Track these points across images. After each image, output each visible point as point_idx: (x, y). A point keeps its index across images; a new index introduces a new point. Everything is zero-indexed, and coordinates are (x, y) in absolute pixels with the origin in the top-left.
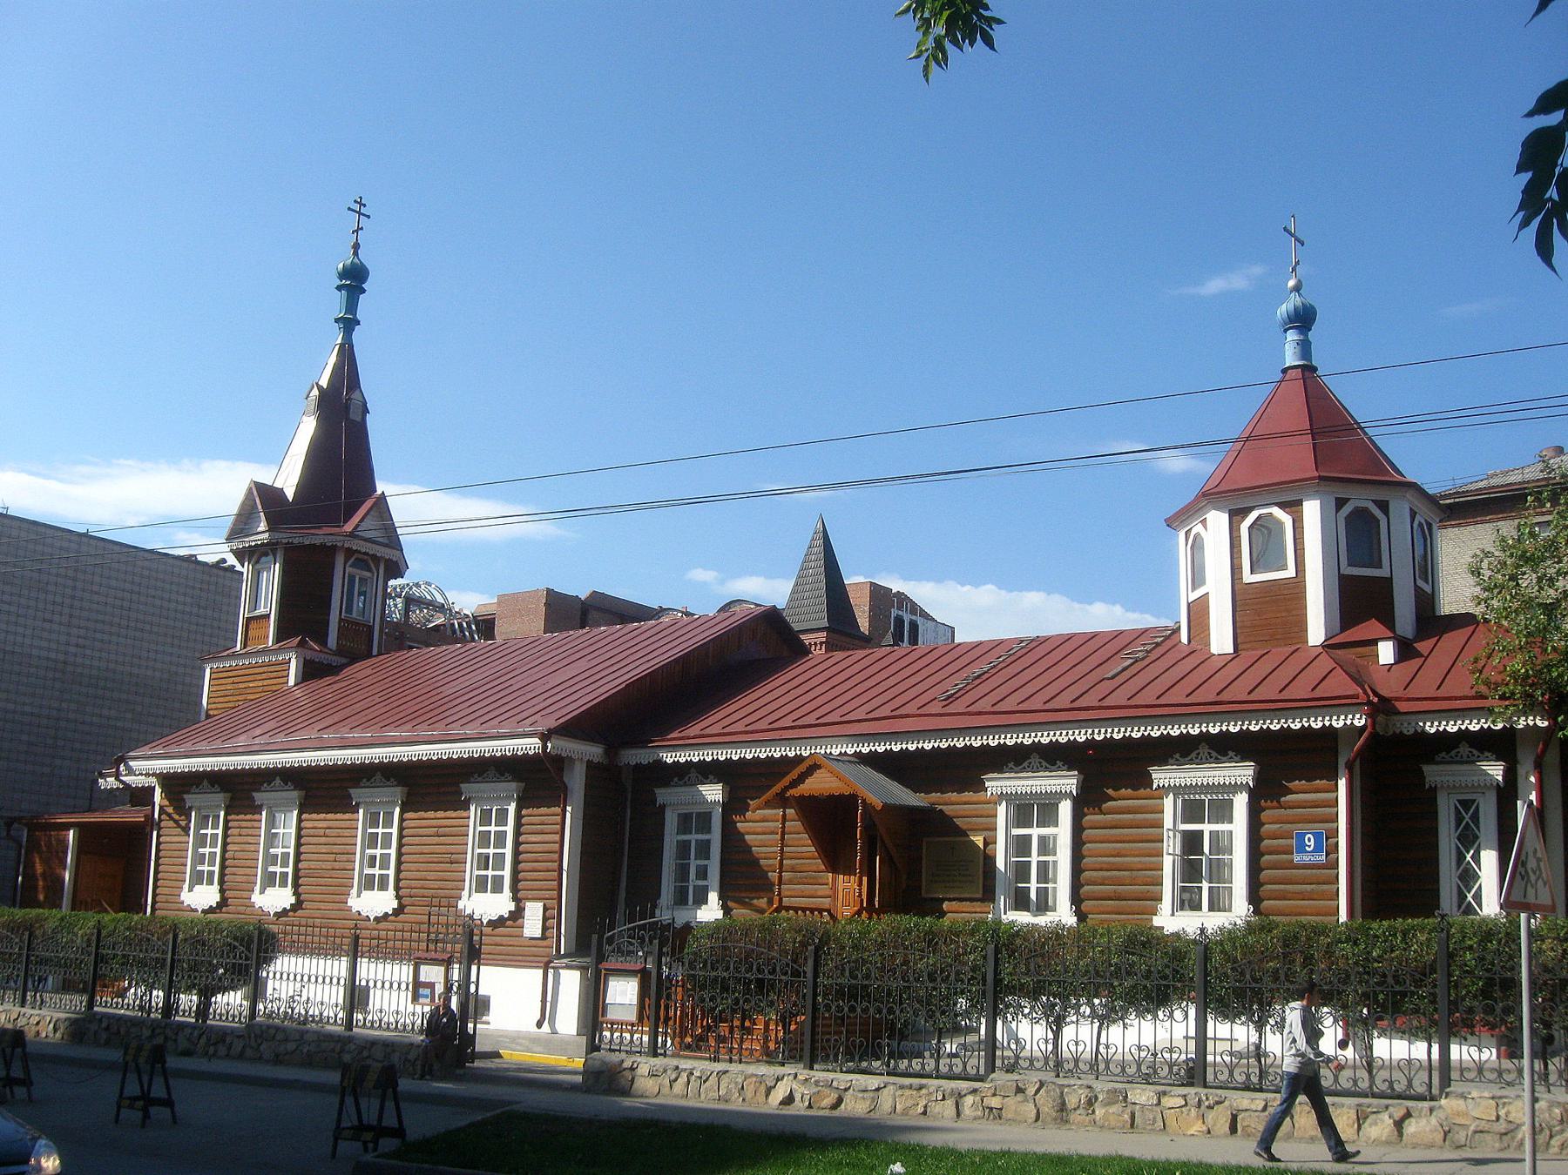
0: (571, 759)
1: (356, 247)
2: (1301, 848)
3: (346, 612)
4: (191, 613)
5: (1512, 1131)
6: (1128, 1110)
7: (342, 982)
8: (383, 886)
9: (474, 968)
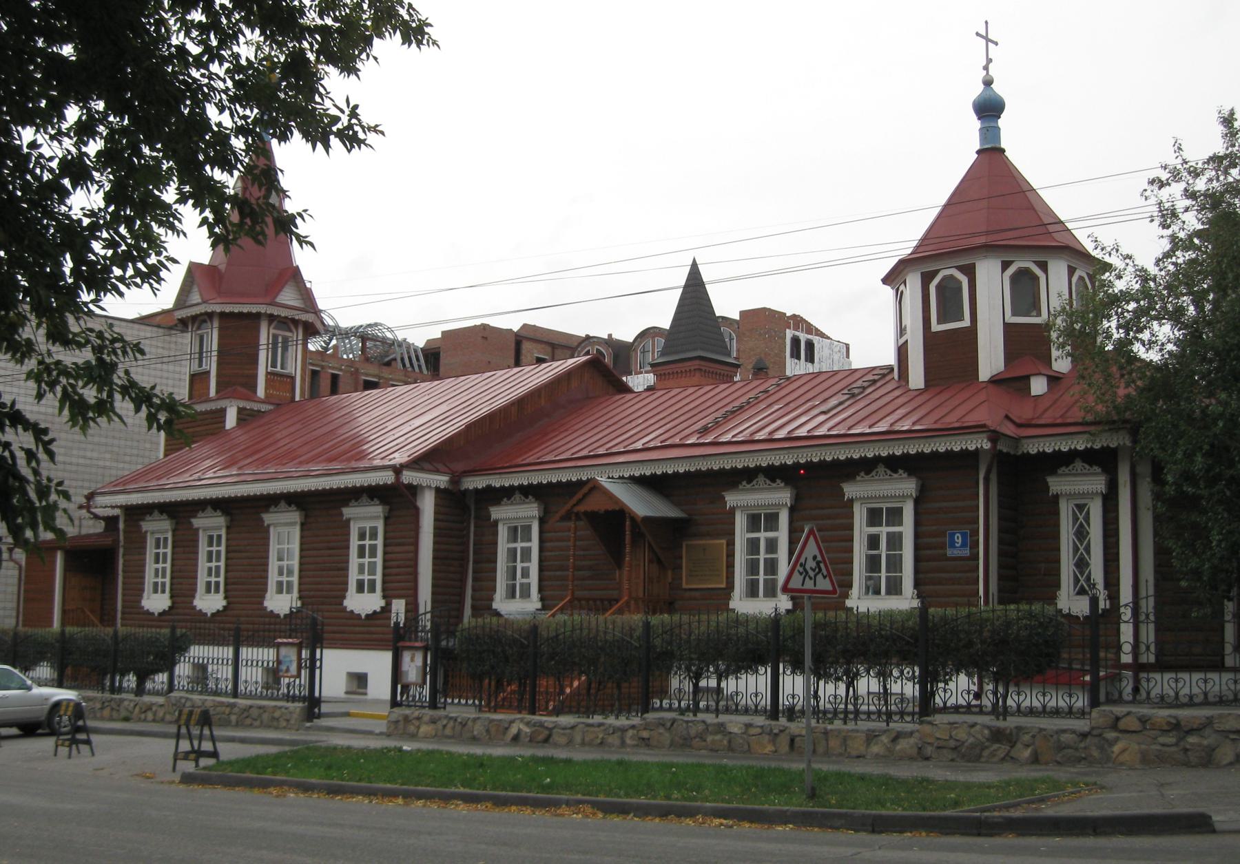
2: (952, 545)
5: (959, 746)
6: (727, 738)
7: (230, 662)
8: (372, 589)
9: (318, 651)
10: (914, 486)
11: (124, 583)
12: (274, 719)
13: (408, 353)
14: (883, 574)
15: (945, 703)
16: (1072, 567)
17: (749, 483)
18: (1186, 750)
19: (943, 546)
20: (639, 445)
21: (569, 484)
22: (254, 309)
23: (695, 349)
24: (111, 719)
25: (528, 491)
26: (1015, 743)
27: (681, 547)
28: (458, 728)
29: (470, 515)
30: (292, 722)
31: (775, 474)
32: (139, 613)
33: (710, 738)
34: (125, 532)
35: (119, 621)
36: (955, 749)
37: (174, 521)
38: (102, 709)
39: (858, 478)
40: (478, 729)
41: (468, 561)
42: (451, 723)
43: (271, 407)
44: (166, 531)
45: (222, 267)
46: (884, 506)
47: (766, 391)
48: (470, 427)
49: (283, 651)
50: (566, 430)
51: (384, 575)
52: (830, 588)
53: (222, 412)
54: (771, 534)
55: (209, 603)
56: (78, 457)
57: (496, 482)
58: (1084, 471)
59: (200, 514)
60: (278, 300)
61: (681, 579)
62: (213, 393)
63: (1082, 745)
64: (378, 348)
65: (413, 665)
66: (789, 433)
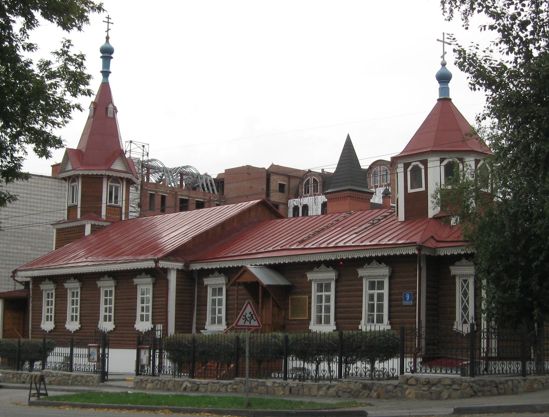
0: (170, 269)
1: (108, 38)
2: (405, 299)
3: (109, 202)
4: (54, 201)
7: (75, 355)
10: (388, 271)
11: (32, 316)
12: (87, 381)
13: (206, 181)
14: (375, 313)
15: (393, 375)
16: (461, 310)
17: (317, 268)
18: (431, 393)
19: (402, 301)
20: (271, 249)
21: (238, 267)
22: (99, 173)
23: (347, 185)
24: (17, 383)
25: (221, 271)
26: (371, 390)
27: (288, 299)
28: (162, 385)
29: (195, 283)
30: (95, 383)
31: (329, 264)
32: (40, 331)
33: (259, 388)
34: (33, 290)
35: (30, 335)
36: (350, 392)
37: (56, 284)
38: (13, 378)
39: (365, 267)
40: (170, 385)
41: (194, 305)
42: (160, 382)
43: (108, 224)
44: (52, 290)
45: (84, 150)
46: (376, 280)
47: (338, 220)
48: (194, 238)
49: (91, 349)
50: (243, 239)
51: (153, 312)
52: (257, 325)
53: (83, 227)
54: (327, 293)
55: (73, 326)
56: (14, 249)
57: (206, 266)
58: (466, 264)
59: (68, 281)
60: (112, 167)
61: (288, 315)
62: (79, 216)
63: (395, 391)
64: (191, 179)
65: (145, 356)
66: (336, 244)
